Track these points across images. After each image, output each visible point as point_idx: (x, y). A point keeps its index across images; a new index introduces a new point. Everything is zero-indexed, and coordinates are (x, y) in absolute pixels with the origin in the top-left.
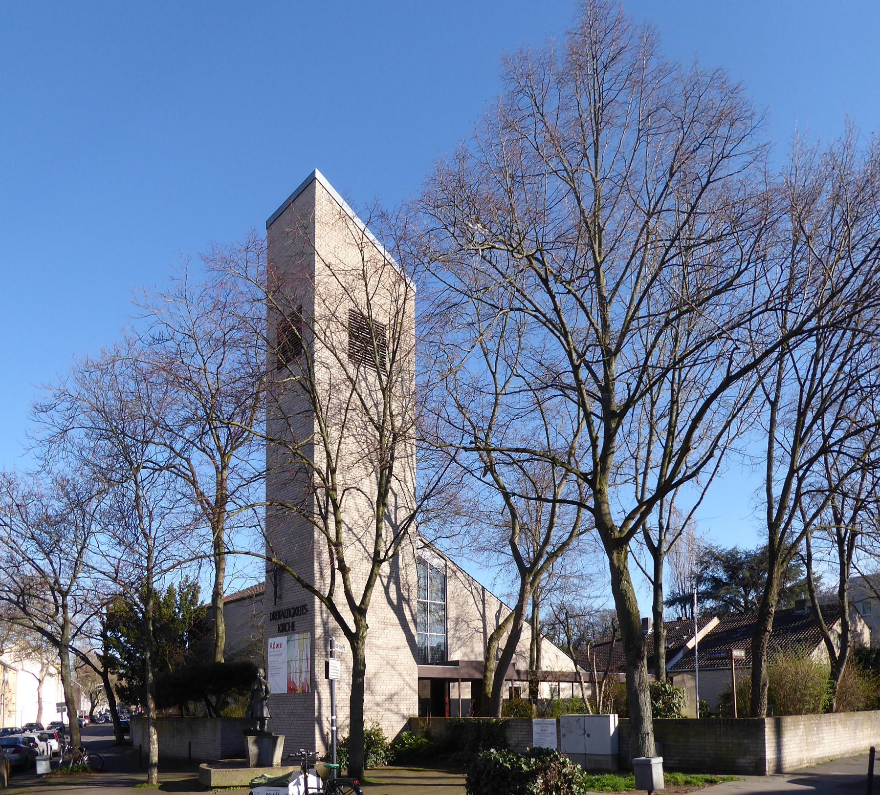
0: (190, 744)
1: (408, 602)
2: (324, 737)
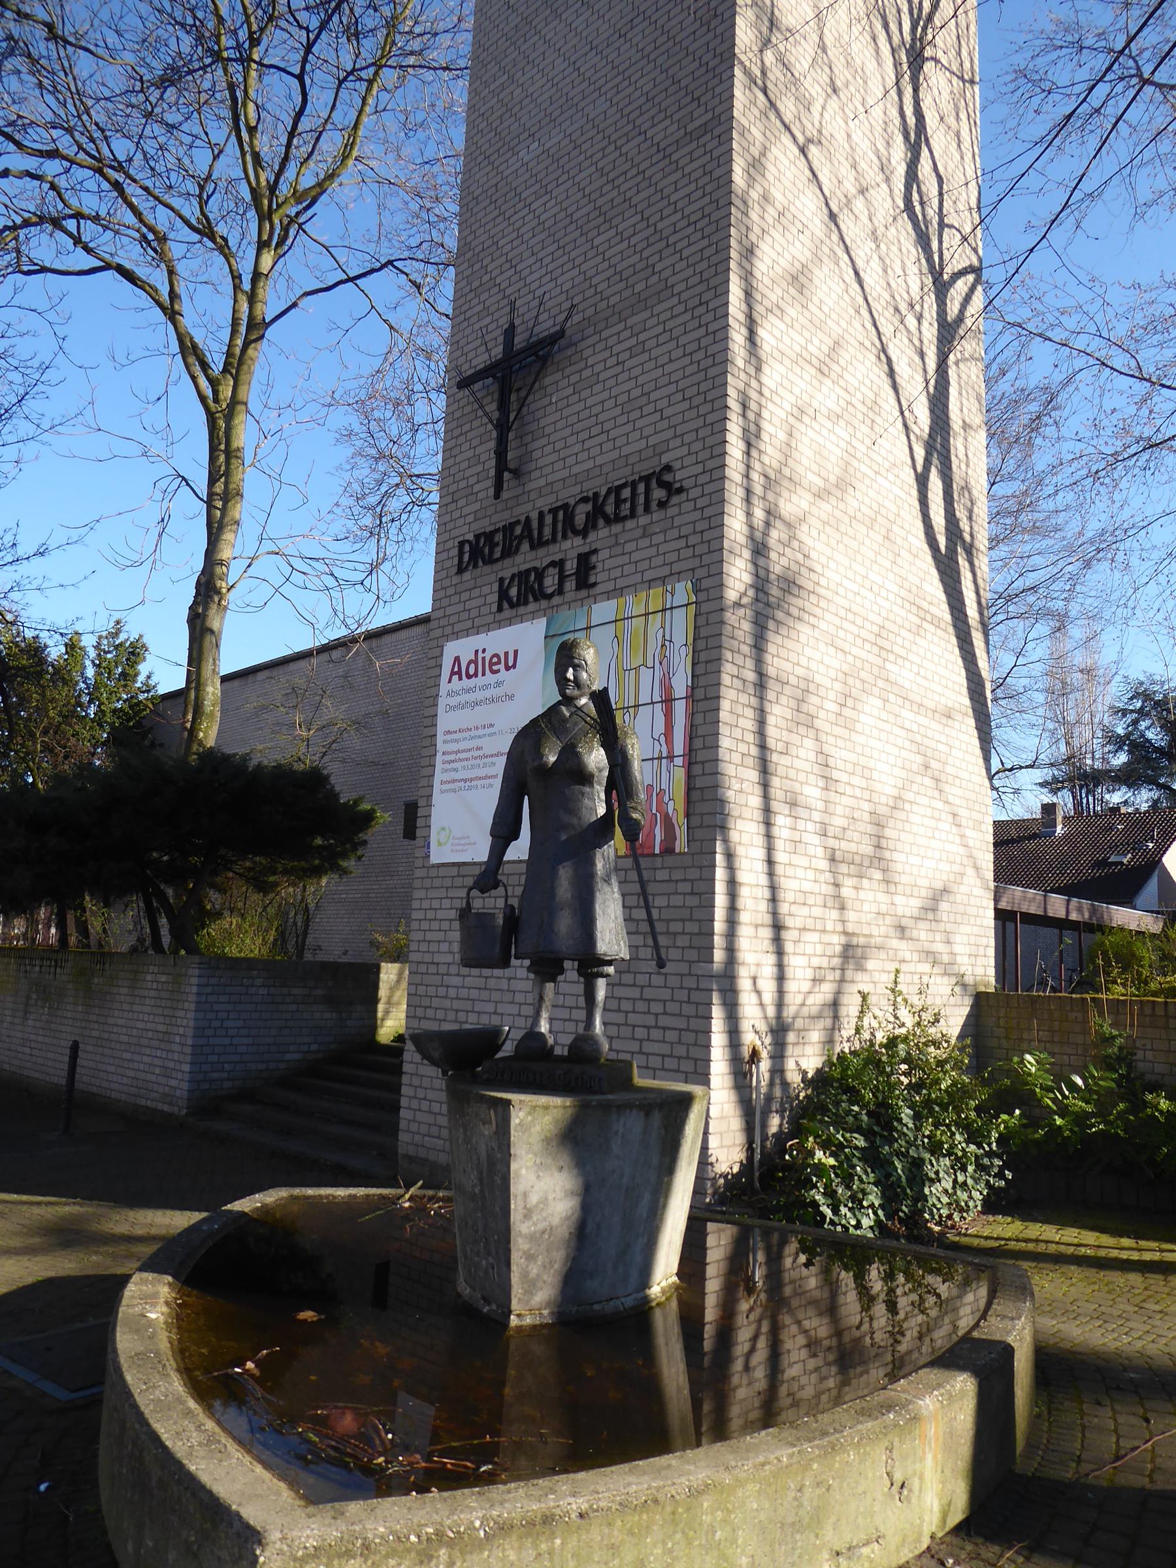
0: (75, 1048)
1: (969, 550)
2: (742, 1067)
